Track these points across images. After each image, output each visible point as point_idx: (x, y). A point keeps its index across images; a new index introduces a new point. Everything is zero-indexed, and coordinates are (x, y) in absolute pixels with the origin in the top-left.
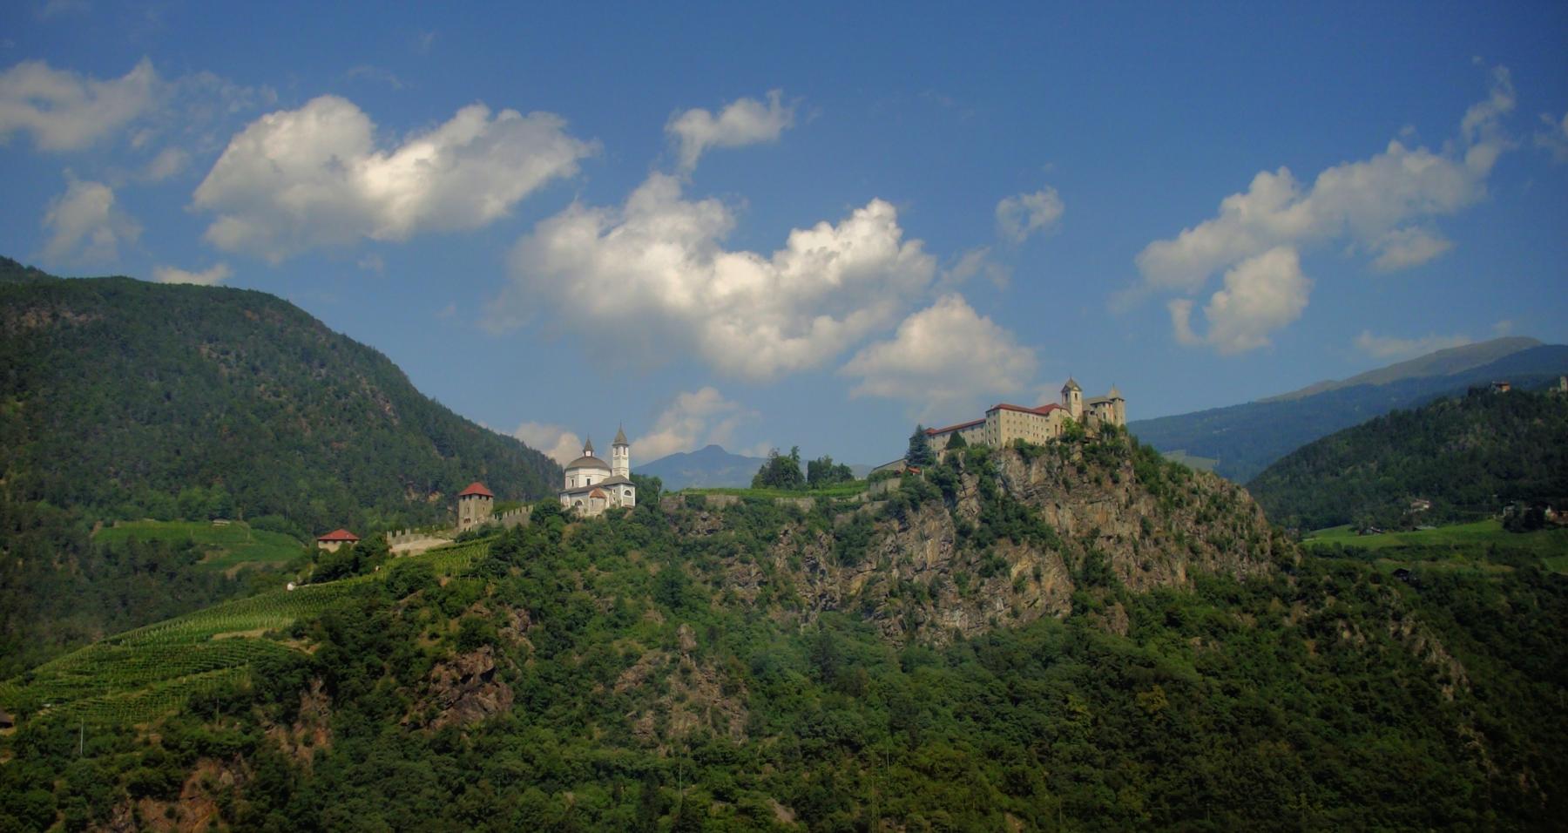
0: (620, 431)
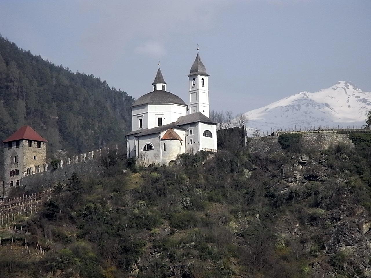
0: (197, 58)
